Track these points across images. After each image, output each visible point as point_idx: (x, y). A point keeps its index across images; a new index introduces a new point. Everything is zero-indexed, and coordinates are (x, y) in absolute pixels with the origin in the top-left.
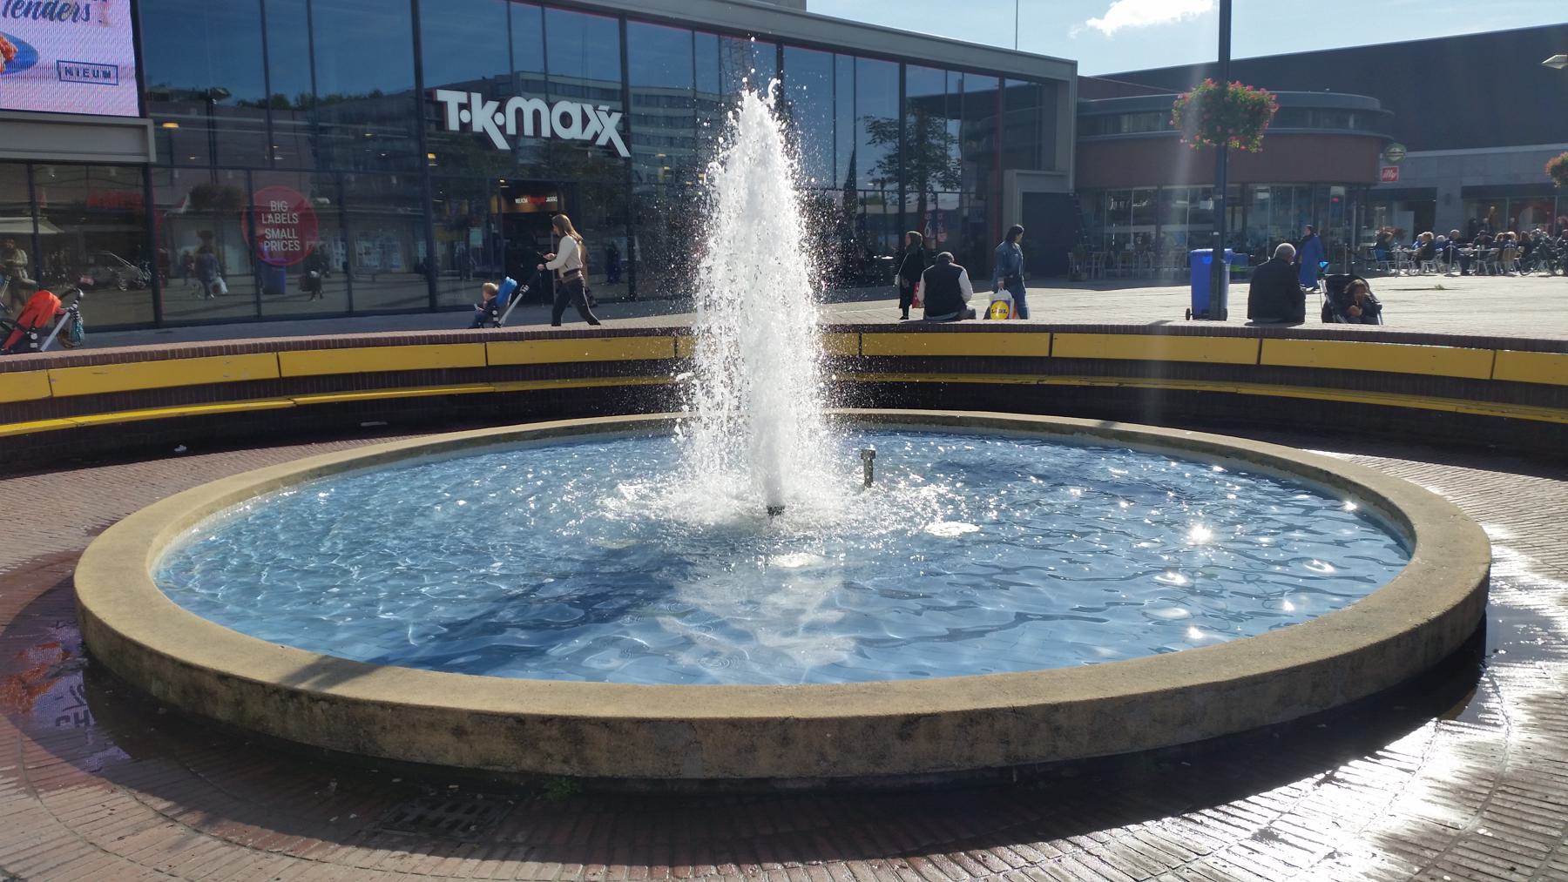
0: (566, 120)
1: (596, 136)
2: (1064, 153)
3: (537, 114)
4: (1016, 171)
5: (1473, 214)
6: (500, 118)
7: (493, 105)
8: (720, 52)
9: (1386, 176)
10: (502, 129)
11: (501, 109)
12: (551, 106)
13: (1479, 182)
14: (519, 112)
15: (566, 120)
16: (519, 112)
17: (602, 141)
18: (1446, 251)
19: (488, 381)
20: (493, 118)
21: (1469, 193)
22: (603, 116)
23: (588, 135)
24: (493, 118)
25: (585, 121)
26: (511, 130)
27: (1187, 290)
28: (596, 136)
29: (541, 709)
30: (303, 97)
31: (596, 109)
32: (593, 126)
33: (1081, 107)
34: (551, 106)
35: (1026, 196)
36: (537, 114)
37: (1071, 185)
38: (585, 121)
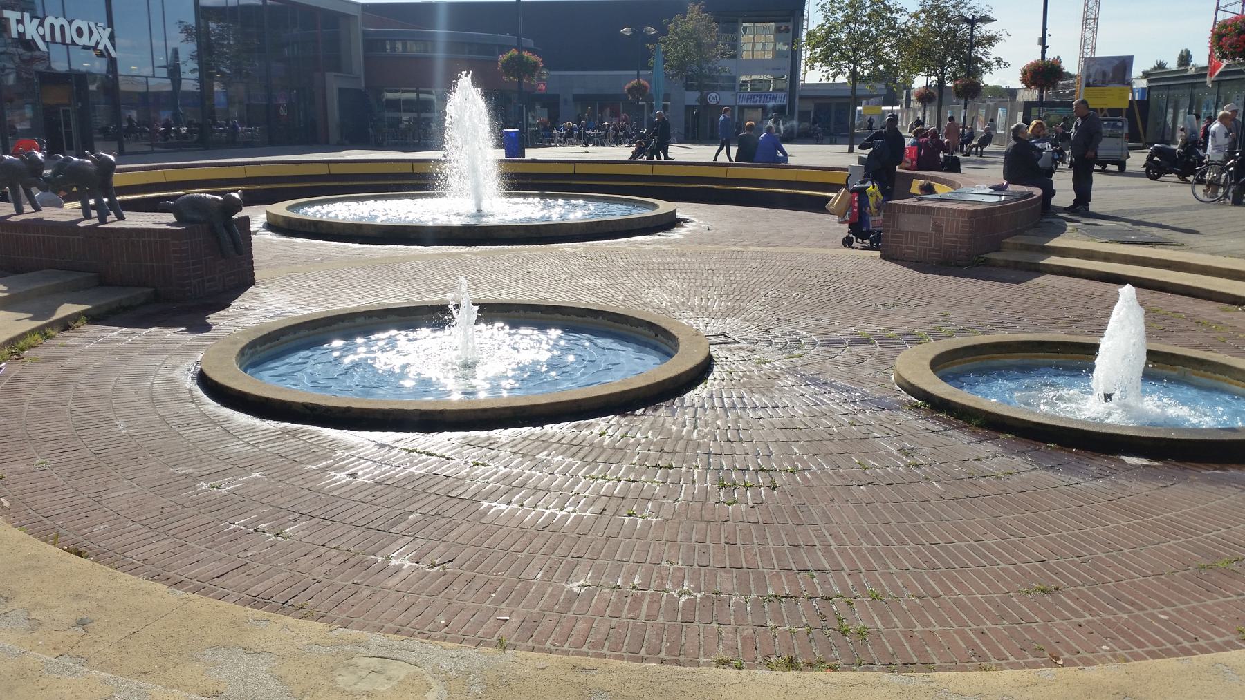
0: (80, 32)
1: (97, 43)
2: (358, 66)
3: (62, 27)
4: (334, 74)
5: (579, 111)
6: (41, 30)
7: (36, 21)
8: (1216, 14)
9: (539, 87)
10: (43, 37)
11: (41, 24)
12: (70, 22)
13: (582, 92)
14: (52, 26)
15: (80, 32)
16: (52, 26)
17: (101, 47)
18: (580, 133)
19: (262, 183)
20: (37, 30)
21: (578, 98)
22: (101, 30)
23: (93, 43)
24: (37, 30)
25: (91, 33)
26: (48, 38)
27: (1052, 203)
28: (97, 43)
29: (364, 302)
30: (1161, 66)
31: (96, 25)
32: (96, 37)
33: (365, 33)
34: (70, 22)
35: (340, 90)
36: (62, 27)
37: (363, 85)
38: (91, 33)
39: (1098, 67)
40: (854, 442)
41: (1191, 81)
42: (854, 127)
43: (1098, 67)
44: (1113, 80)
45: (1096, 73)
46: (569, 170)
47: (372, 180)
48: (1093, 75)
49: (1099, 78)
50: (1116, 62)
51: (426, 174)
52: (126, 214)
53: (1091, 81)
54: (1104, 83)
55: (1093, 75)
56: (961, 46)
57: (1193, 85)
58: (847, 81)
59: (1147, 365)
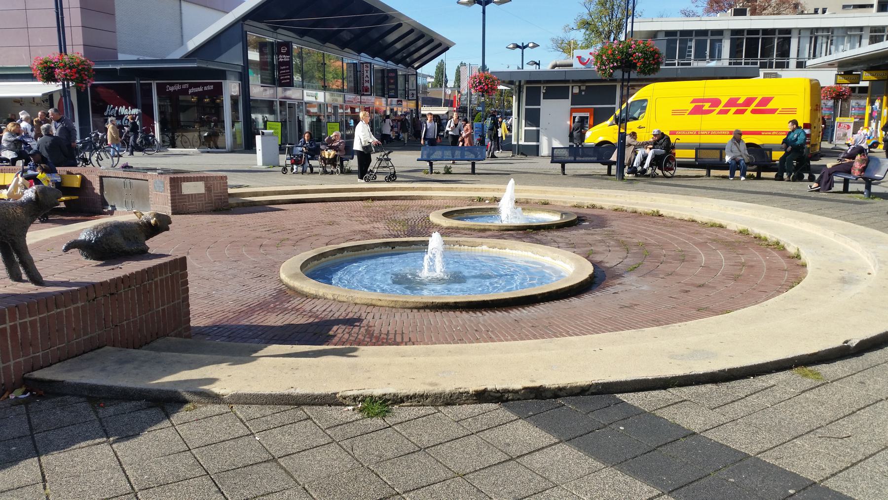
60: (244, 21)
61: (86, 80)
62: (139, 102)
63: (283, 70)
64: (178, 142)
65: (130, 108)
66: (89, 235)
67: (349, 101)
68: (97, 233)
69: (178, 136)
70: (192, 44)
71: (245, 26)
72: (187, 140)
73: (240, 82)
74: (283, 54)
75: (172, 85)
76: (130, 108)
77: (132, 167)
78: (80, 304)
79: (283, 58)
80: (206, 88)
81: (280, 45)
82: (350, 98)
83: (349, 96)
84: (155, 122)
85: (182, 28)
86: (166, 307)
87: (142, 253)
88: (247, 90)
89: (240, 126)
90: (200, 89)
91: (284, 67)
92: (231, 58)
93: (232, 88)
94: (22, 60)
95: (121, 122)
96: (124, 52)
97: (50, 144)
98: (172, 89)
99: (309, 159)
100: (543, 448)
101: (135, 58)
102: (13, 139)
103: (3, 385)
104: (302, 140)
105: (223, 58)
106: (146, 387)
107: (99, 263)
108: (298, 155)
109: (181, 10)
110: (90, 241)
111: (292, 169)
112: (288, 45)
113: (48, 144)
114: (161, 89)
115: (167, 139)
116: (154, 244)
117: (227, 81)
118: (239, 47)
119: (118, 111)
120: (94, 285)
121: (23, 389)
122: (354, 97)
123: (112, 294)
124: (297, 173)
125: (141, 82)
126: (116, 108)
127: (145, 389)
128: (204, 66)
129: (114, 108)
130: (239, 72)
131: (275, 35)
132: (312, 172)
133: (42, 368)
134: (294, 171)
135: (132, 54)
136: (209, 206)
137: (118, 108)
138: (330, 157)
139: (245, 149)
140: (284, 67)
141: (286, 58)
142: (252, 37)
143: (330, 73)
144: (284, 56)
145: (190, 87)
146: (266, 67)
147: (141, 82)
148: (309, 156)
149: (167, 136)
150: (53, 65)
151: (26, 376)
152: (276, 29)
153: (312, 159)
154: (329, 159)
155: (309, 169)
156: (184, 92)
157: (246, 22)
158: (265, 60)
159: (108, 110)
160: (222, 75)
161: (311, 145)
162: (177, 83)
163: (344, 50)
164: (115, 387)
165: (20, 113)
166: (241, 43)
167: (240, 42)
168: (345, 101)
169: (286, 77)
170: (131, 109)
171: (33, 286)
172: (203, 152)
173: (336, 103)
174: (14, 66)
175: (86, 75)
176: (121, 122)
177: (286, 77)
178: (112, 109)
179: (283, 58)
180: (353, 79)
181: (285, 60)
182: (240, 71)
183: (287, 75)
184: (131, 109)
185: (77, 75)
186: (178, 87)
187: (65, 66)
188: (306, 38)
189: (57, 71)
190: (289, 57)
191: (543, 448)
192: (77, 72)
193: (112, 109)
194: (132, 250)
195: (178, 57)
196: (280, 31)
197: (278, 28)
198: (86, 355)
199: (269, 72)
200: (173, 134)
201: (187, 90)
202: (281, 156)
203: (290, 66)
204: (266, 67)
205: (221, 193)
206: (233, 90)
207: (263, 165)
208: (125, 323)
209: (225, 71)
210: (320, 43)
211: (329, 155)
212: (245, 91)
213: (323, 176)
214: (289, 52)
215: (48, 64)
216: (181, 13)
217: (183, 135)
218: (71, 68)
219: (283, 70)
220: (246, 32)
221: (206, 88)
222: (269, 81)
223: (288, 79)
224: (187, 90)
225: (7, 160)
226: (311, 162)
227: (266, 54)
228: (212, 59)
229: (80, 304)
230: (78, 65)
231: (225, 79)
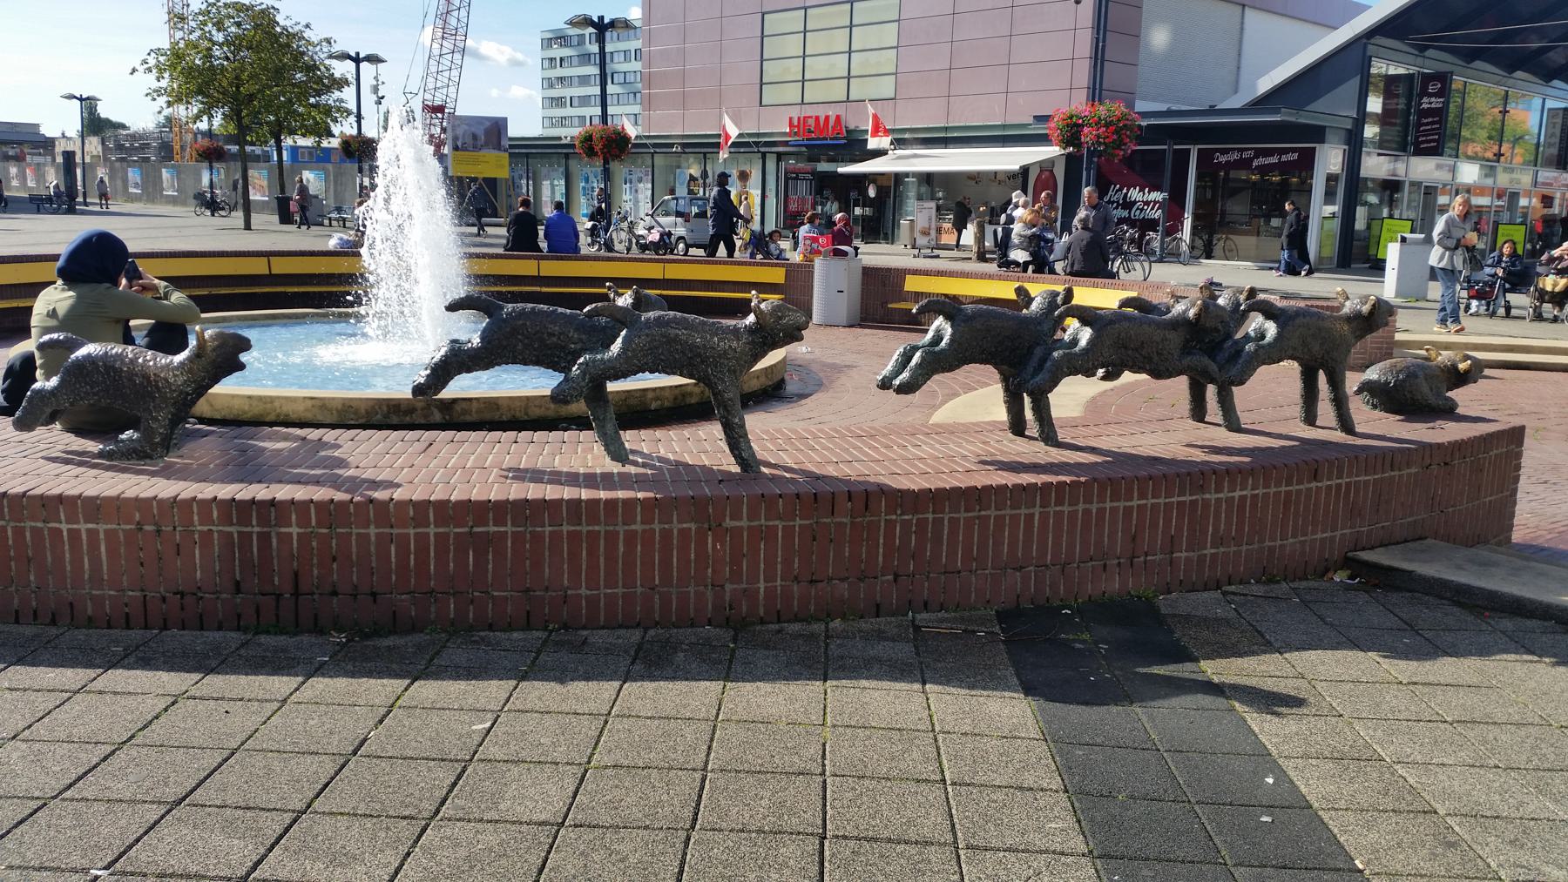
39: (466, 127)
40: (753, 342)
41: (564, 151)
42: (163, 189)
43: (466, 127)
44: (486, 145)
45: (464, 135)
46: (258, 267)
47: (529, 285)
48: (461, 137)
49: (469, 140)
50: (488, 124)
51: (351, 276)
52: (1013, 296)
53: (459, 144)
54: (476, 148)
55: (461, 137)
56: (205, 56)
57: (567, 156)
58: (592, 223)
59: (1373, 180)
60: (1368, 39)
61: (1125, 144)
62: (1167, 181)
63: (1427, 124)
64: (1218, 249)
65: (1147, 190)
66: (1384, 374)
67: (1544, 184)
68: (1398, 373)
69: (1219, 240)
70: (1265, 84)
71: (1370, 47)
72: (1234, 247)
73: (1346, 147)
74: (1431, 95)
75: (1224, 152)
76: (1147, 190)
77: (1221, 285)
78: (1413, 470)
79: (1430, 103)
80: (1284, 158)
81: (1427, 79)
82: (1548, 178)
83: (1547, 174)
84: (1186, 216)
85: (1239, 55)
86: (1135, 503)
87: (1448, 411)
88: (1356, 161)
89: (1335, 225)
90: (1274, 160)
91: (1430, 120)
92: (1334, 106)
93: (1331, 159)
94: (1021, 114)
95: (1130, 213)
96: (1145, 98)
97: (1088, 243)
98: (1223, 159)
99: (1506, 291)
100: (146, 833)
101: (1163, 107)
102: (1029, 232)
103: (1326, 560)
104: (1495, 254)
105: (1319, 105)
106: (1558, 603)
107: (1398, 417)
108: (1485, 283)
109: (1242, 23)
110: (1387, 383)
111: (1468, 308)
112: (1443, 78)
113: (1085, 242)
114: (1204, 157)
115: (1199, 243)
116: (1463, 398)
117: (1326, 146)
118: (1354, 84)
119: (1126, 194)
120: (1430, 445)
121: (1349, 572)
122: (1555, 174)
123: (1446, 464)
124: (1476, 314)
125: (1175, 147)
126: (1125, 191)
127: (1557, 606)
128: (1292, 119)
129: (1121, 190)
130: (1347, 130)
131: (1420, 60)
132: (1508, 315)
133: (1372, 548)
134: (1472, 311)
135: (1154, 100)
136: (1358, 359)
137: (1128, 190)
138: (1557, 289)
139: (1338, 267)
140: (1430, 120)
141: (1436, 103)
142: (1379, 68)
143: (1483, 128)
144: (1433, 99)
145: (1256, 156)
146: (1394, 121)
147: (1175, 147)
148: (1507, 286)
149: (1201, 238)
150: (1081, 121)
151: (1350, 554)
152: (1422, 49)
153: (1512, 290)
154: (1552, 292)
155: (1502, 311)
156: (1244, 164)
157: (1373, 41)
158: (1394, 107)
159: (1110, 193)
160: (1318, 134)
161: (1513, 265)
162: (1234, 149)
163: (1550, 84)
164: (1503, 594)
165: (1014, 194)
166: (1359, 77)
167: (1356, 75)
168: (1535, 183)
169: (1431, 137)
170: (1149, 192)
171: (1343, 434)
172: (1262, 269)
173: (1516, 186)
174: (962, 124)
175: (1127, 136)
176: (1130, 213)
177: (1431, 137)
178: (1117, 191)
179: (1430, 103)
180: (1558, 140)
181: (1433, 106)
182: (1349, 127)
183: (1433, 135)
184: (1149, 192)
185: (1115, 137)
186: (1236, 156)
187: (1098, 123)
188: (1478, 64)
189: (1086, 130)
190: (1442, 100)
191: (146, 833)
192: (1117, 132)
193: (1117, 191)
194: (1439, 405)
195: (1238, 105)
196: (1431, 53)
197: (1427, 47)
198: (1410, 545)
199: (1398, 128)
200: (1211, 236)
201: (1251, 160)
202: (1432, 284)
203: (1441, 118)
204: (1394, 121)
205: (1383, 337)
206: (1332, 161)
207: (1396, 297)
208: (1450, 510)
209: (1324, 128)
210: (1505, 74)
211: (1555, 285)
212: (1353, 168)
213: (1537, 325)
214: (1444, 92)
215: (1074, 119)
216: (1242, 29)
217: (1227, 238)
218: (1107, 125)
219: (1427, 124)
220: (1371, 57)
221: (1284, 158)
222: (1394, 146)
223: (1433, 141)
224: (1251, 160)
225: (1017, 264)
226: (1509, 296)
227: (1397, 96)
228: (1299, 106)
229: (1413, 470)
230: (1119, 120)
231: (1322, 141)
